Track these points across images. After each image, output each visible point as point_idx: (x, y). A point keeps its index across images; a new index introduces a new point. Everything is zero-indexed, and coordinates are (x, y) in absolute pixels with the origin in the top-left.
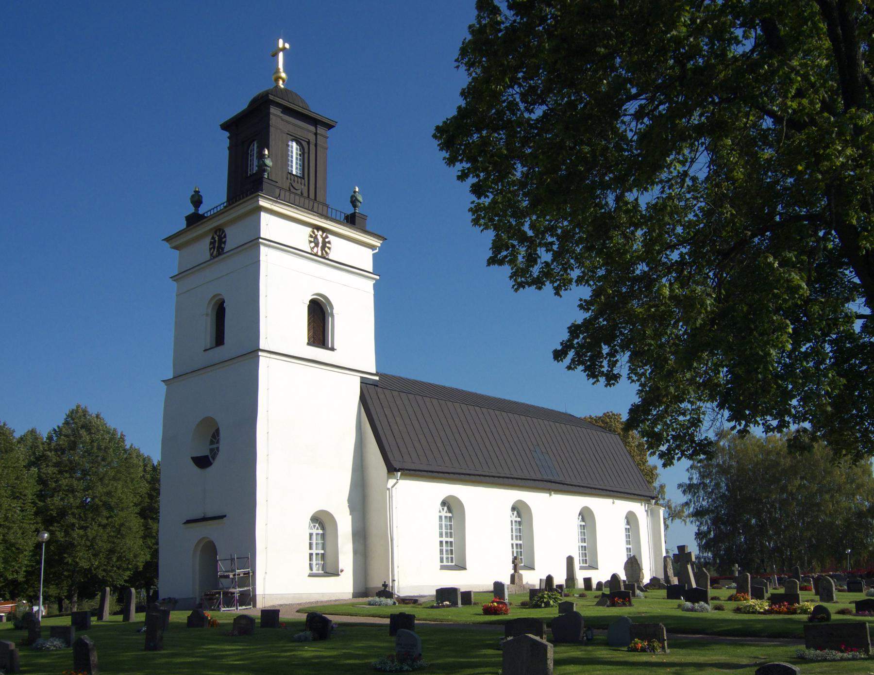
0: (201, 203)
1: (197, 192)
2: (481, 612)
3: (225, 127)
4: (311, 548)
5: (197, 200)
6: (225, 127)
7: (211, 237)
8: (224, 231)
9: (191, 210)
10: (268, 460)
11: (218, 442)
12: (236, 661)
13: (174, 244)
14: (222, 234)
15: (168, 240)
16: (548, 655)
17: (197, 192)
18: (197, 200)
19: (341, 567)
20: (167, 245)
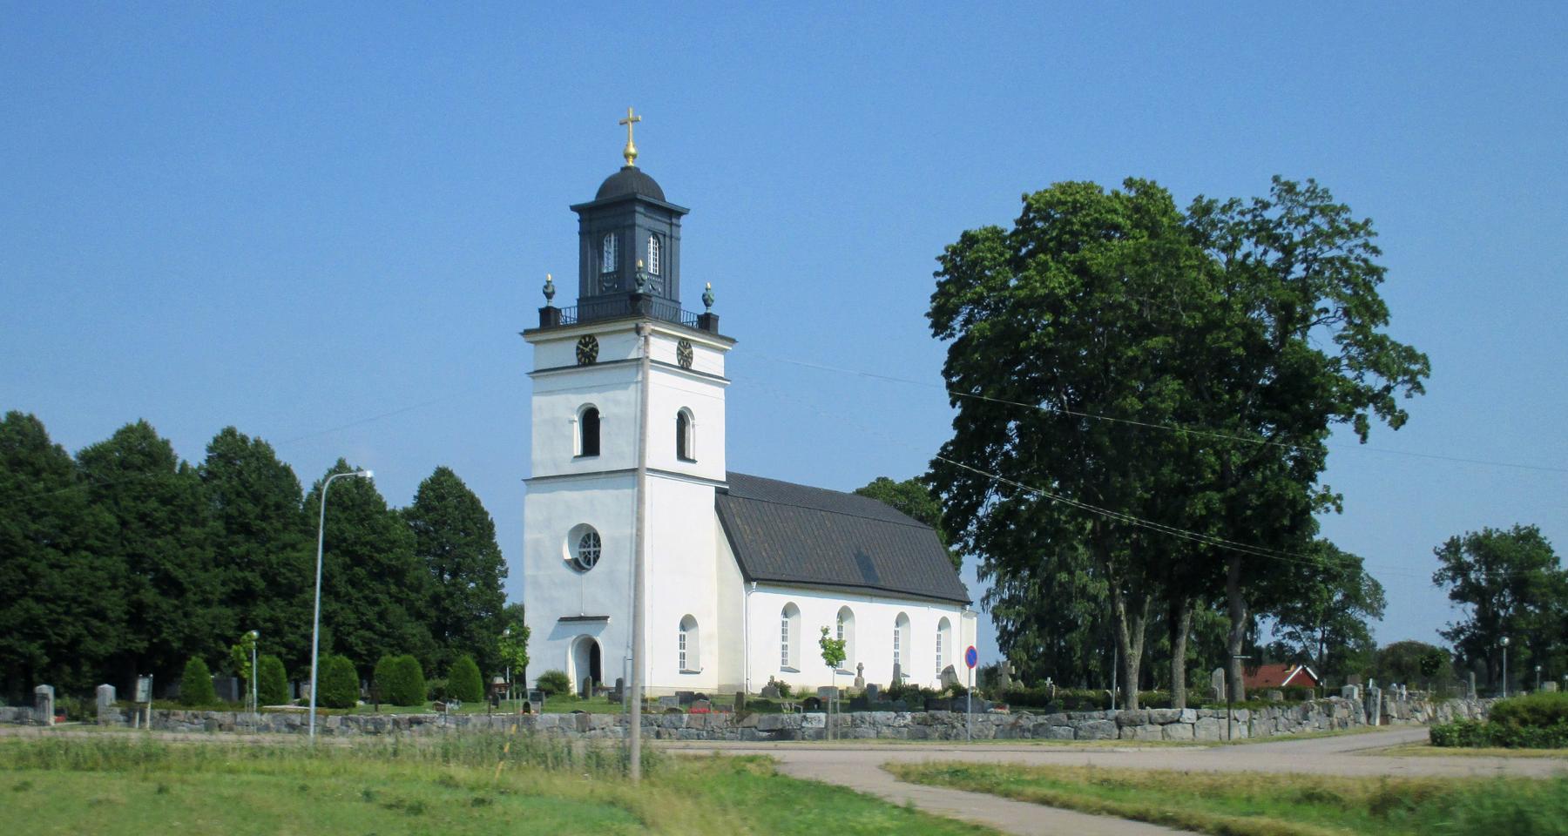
11: (600, 546)
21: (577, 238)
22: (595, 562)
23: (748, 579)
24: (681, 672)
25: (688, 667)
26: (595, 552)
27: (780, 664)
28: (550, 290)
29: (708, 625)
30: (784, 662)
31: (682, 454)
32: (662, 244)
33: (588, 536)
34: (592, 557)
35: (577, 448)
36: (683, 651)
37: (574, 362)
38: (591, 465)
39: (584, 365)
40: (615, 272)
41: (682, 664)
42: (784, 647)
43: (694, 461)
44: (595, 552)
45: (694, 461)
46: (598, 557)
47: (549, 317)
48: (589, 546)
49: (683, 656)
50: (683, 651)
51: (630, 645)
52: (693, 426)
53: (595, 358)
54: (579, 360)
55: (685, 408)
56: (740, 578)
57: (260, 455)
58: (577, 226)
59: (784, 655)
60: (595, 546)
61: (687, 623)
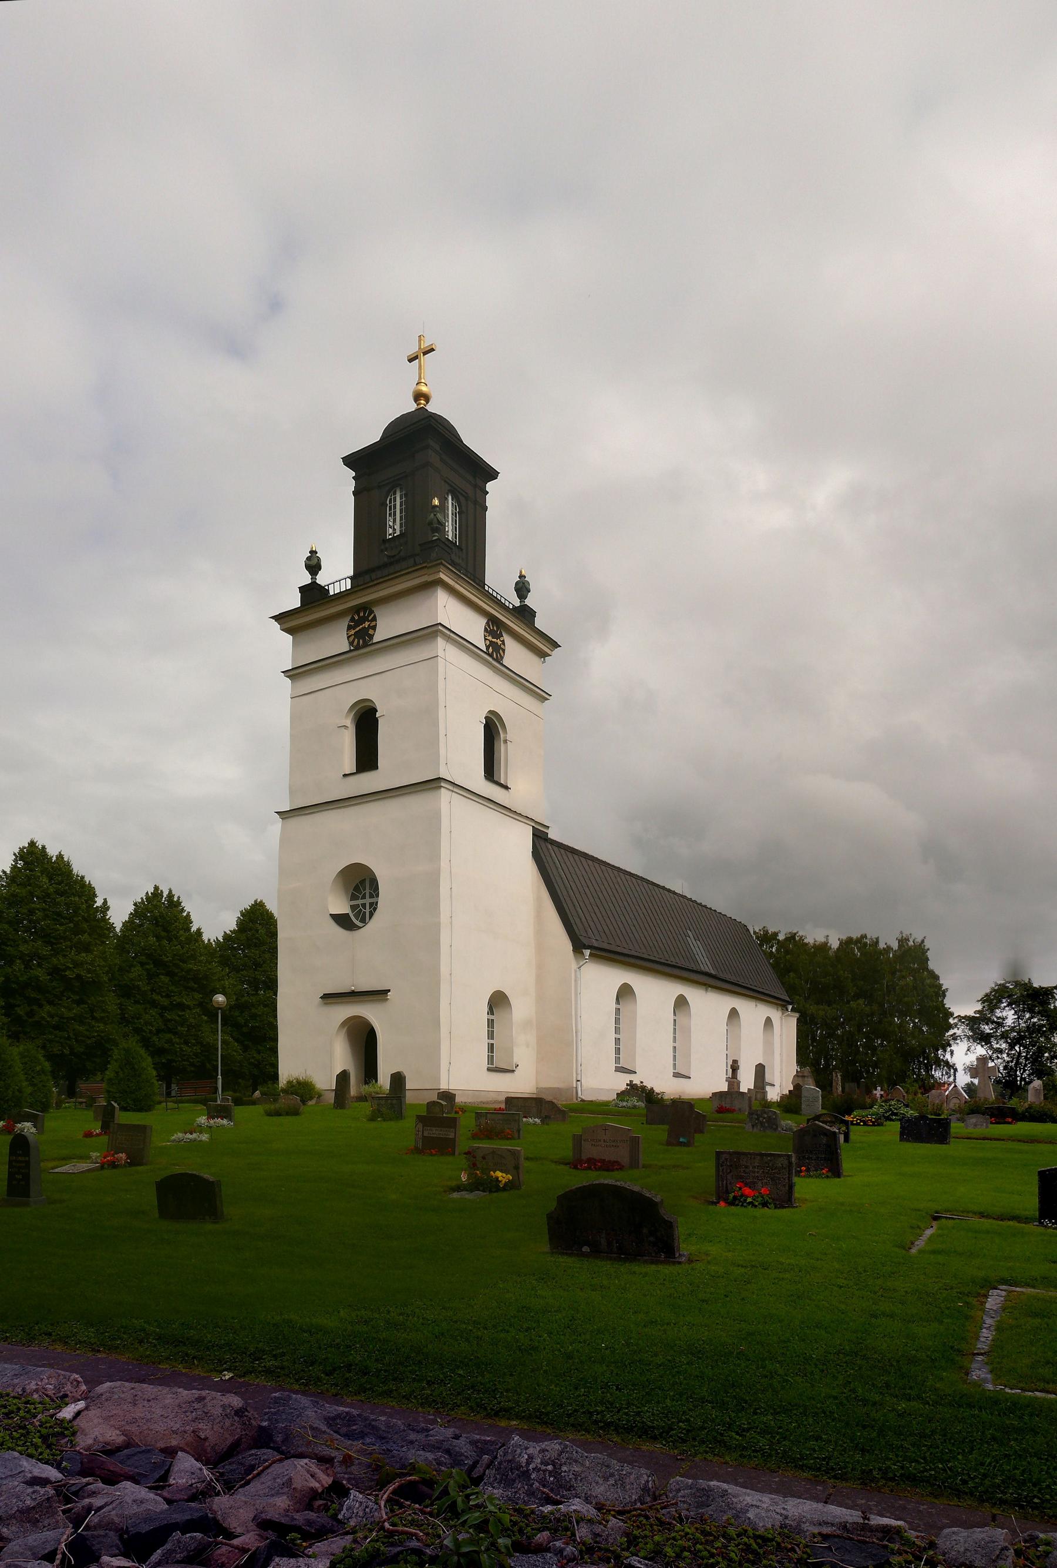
0: (320, 568)
1: (313, 552)
2: (1030, 1201)
3: (350, 461)
4: (488, 1027)
5: (313, 565)
6: (350, 461)
7: (349, 618)
8: (372, 612)
9: (306, 579)
10: (451, 923)
11: (378, 896)
12: (101, 1456)
13: (287, 625)
14: (369, 615)
15: (278, 618)
16: (206, 1176)
17: (313, 552)
18: (313, 565)
19: (515, 1060)
20: (276, 626)
21: (352, 499)
22: (371, 915)
23: (578, 947)
24: (489, 1070)
25: (498, 1063)
26: (371, 904)
27: (672, 1071)
28: (314, 562)
29: (521, 1008)
30: (617, 1060)
31: (490, 771)
32: (464, 508)
33: (363, 882)
34: (368, 911)
35: (348, 760)
36: (491, 1041)
37: (345, 646)
38: (369, 782)
39: (357, 648)
40: (402, 534)
41: (491, 1059)
42: (617, 1041)
43: (506, 788)
44: (371, 904)
45: (506, 788)
46: (375, 909)
47: (313, 594)
48: (364, 897)
49: (491, 1048)
50: (491, 1041)
51: (783, 1003)
52: (505, 741)
53: (371, 637)
54: (351, 644)
55: (490, 712)
56: (568, 946)
57: (174, 904)
58: (351, 485)
59: (618, 1051)
60: (371, 896)
61: (498, 1002)
